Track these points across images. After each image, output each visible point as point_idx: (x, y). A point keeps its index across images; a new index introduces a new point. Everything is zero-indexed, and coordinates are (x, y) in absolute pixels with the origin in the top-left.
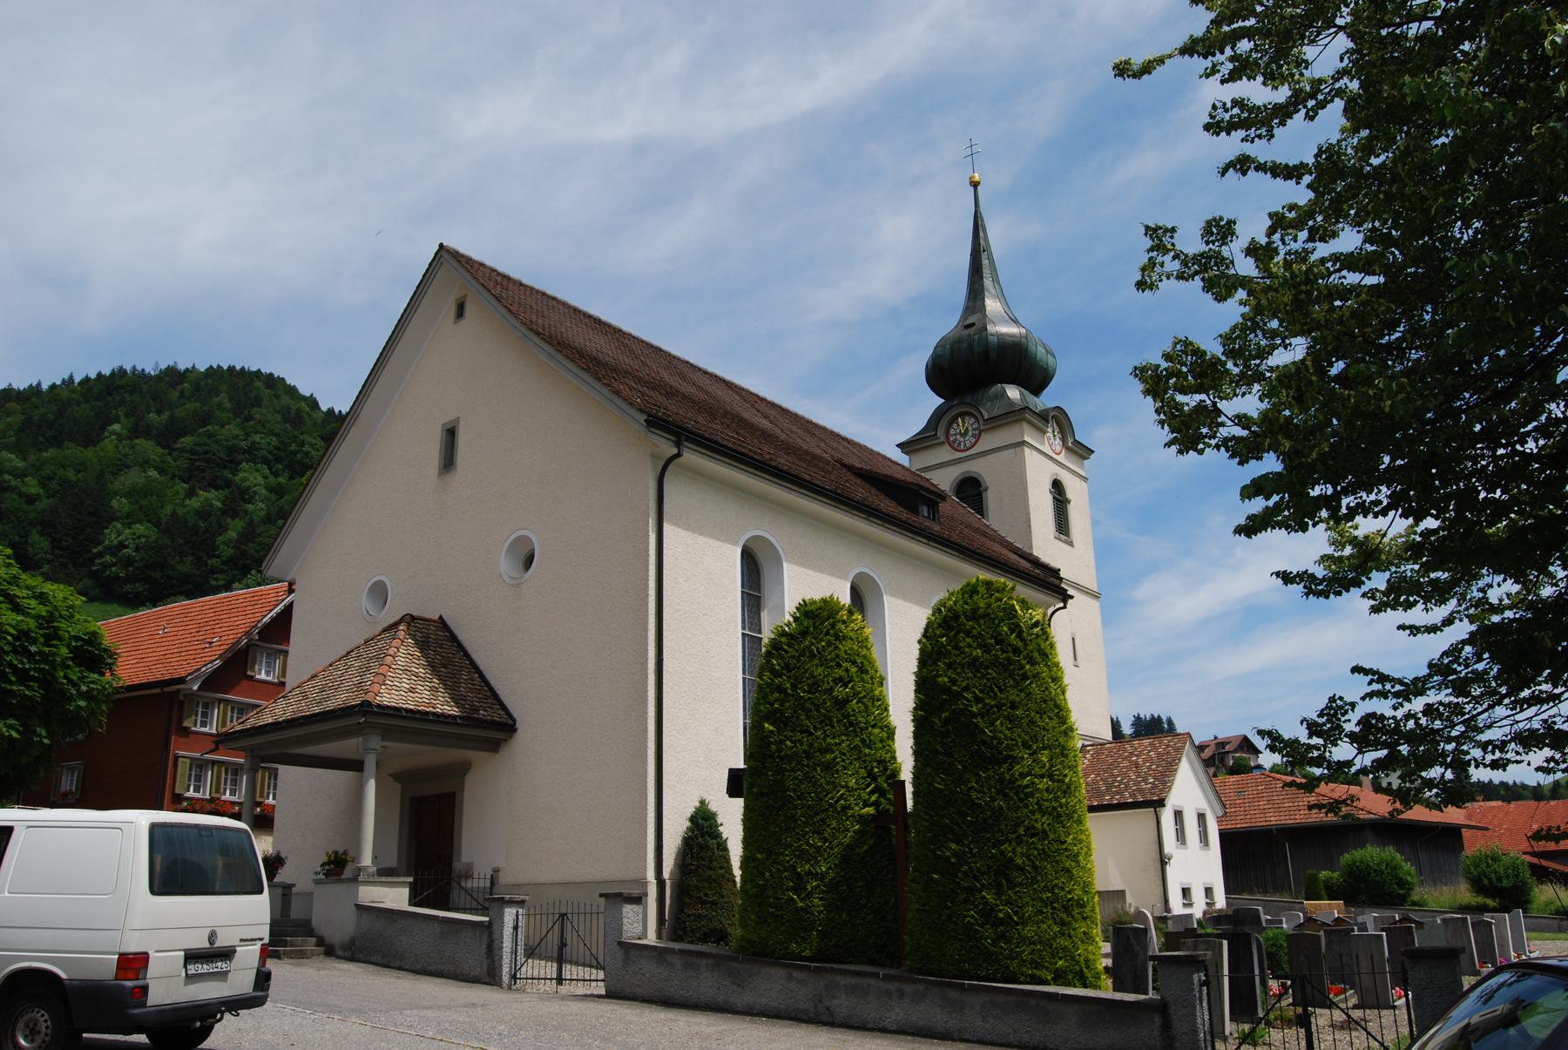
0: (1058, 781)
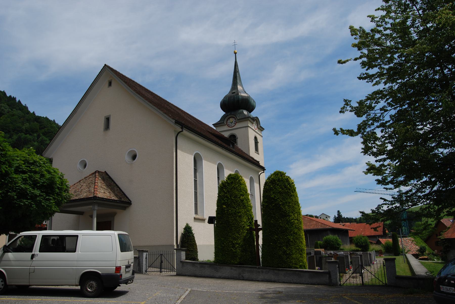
0: (299, 221)
